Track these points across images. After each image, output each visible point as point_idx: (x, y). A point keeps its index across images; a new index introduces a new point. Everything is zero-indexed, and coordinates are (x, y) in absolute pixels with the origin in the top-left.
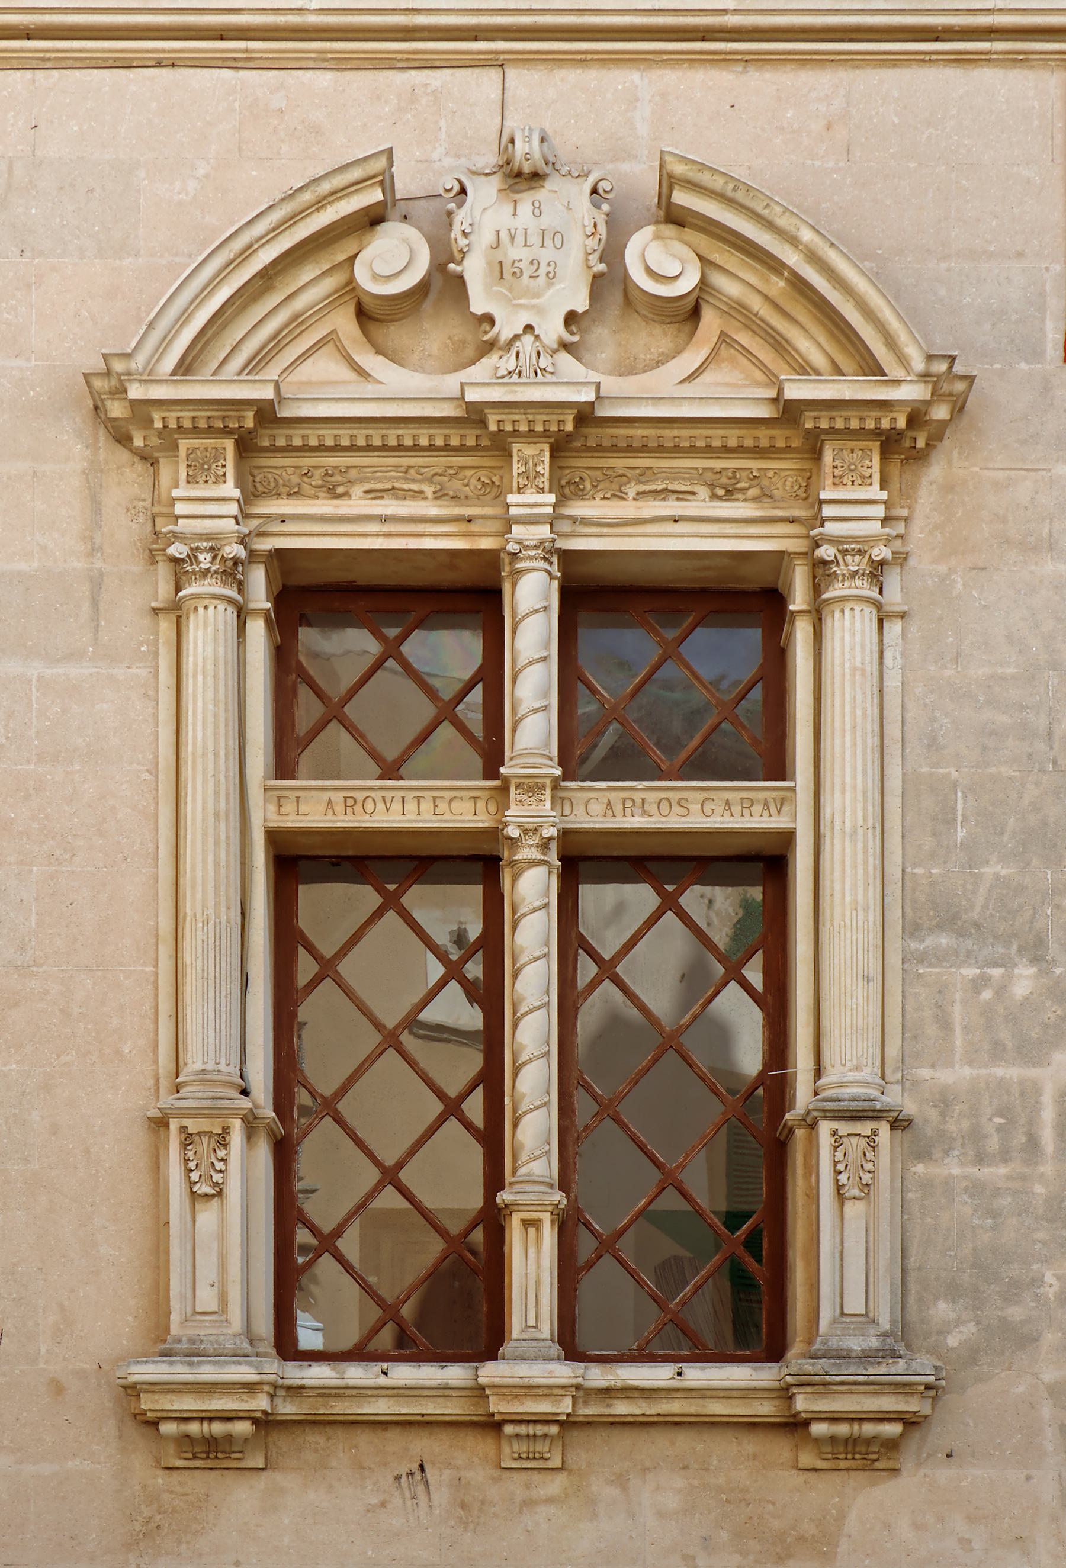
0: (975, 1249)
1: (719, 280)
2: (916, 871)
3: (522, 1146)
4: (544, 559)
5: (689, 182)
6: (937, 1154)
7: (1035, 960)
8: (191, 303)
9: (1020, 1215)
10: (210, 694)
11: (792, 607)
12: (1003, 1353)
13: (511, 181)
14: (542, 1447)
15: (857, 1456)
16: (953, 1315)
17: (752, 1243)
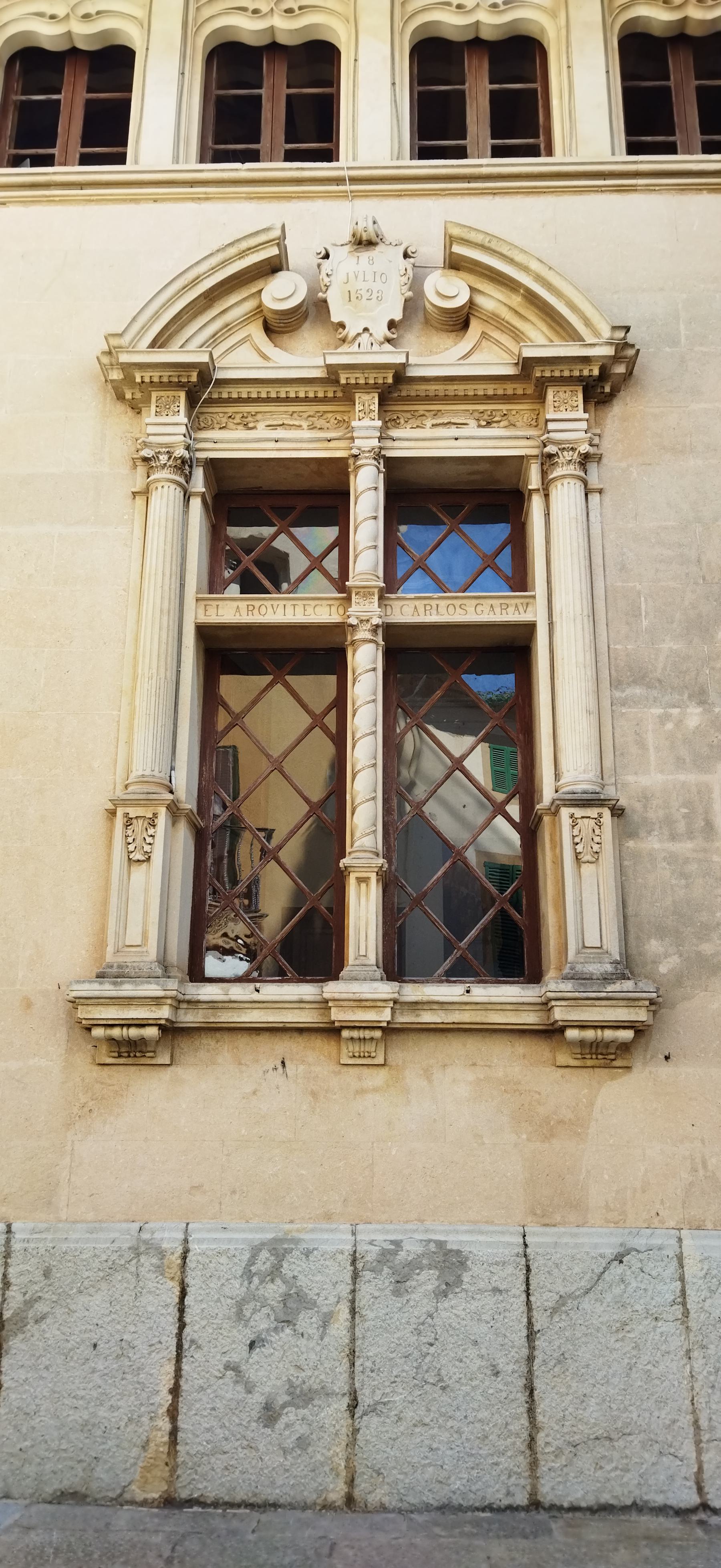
0: (674, 901)
1: (480, 300)
2: (617, 647)
3: (357, 826)
4: (375, 458)
5: (462, 239)
6: (642, 834)
7: (701, 703)
8: (161, 308)
9: (704, 877)
10: (162, 538)
11: (530, 487)
12: (701, 979)
13: (355, 247)
14: (370, 1047)
15: (600, 1057)
16: (661, 950)
17: (515, 902)
